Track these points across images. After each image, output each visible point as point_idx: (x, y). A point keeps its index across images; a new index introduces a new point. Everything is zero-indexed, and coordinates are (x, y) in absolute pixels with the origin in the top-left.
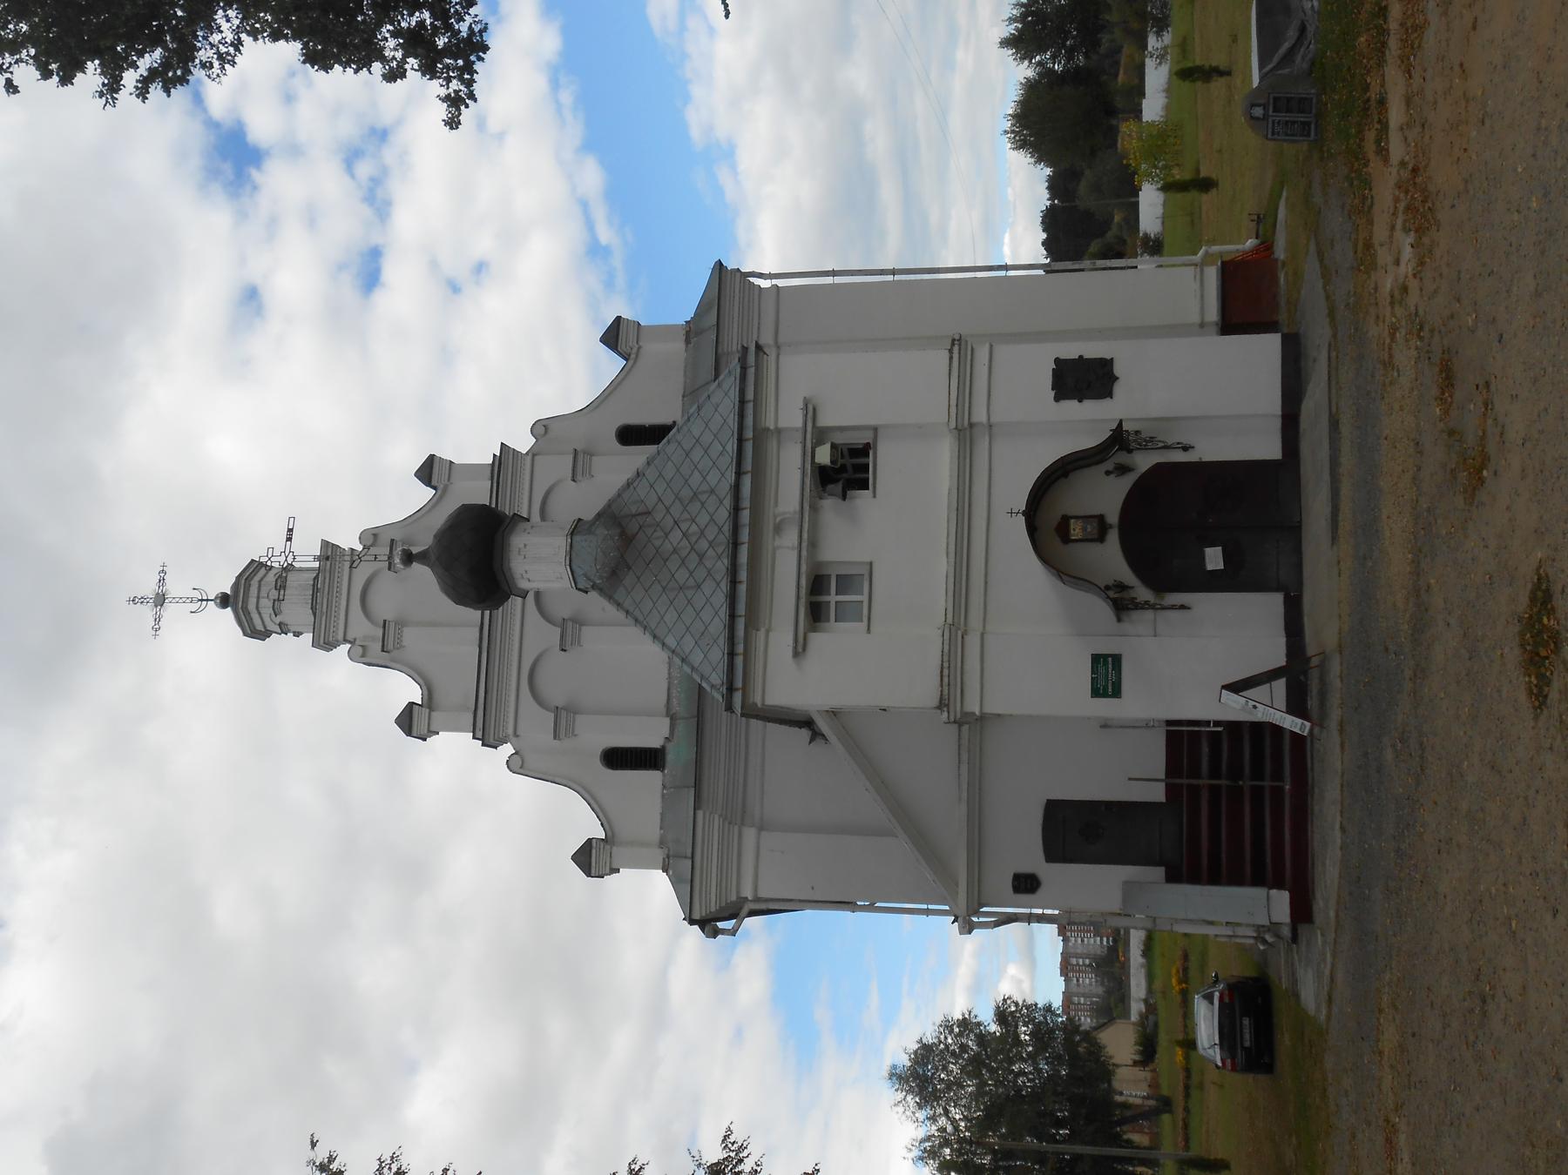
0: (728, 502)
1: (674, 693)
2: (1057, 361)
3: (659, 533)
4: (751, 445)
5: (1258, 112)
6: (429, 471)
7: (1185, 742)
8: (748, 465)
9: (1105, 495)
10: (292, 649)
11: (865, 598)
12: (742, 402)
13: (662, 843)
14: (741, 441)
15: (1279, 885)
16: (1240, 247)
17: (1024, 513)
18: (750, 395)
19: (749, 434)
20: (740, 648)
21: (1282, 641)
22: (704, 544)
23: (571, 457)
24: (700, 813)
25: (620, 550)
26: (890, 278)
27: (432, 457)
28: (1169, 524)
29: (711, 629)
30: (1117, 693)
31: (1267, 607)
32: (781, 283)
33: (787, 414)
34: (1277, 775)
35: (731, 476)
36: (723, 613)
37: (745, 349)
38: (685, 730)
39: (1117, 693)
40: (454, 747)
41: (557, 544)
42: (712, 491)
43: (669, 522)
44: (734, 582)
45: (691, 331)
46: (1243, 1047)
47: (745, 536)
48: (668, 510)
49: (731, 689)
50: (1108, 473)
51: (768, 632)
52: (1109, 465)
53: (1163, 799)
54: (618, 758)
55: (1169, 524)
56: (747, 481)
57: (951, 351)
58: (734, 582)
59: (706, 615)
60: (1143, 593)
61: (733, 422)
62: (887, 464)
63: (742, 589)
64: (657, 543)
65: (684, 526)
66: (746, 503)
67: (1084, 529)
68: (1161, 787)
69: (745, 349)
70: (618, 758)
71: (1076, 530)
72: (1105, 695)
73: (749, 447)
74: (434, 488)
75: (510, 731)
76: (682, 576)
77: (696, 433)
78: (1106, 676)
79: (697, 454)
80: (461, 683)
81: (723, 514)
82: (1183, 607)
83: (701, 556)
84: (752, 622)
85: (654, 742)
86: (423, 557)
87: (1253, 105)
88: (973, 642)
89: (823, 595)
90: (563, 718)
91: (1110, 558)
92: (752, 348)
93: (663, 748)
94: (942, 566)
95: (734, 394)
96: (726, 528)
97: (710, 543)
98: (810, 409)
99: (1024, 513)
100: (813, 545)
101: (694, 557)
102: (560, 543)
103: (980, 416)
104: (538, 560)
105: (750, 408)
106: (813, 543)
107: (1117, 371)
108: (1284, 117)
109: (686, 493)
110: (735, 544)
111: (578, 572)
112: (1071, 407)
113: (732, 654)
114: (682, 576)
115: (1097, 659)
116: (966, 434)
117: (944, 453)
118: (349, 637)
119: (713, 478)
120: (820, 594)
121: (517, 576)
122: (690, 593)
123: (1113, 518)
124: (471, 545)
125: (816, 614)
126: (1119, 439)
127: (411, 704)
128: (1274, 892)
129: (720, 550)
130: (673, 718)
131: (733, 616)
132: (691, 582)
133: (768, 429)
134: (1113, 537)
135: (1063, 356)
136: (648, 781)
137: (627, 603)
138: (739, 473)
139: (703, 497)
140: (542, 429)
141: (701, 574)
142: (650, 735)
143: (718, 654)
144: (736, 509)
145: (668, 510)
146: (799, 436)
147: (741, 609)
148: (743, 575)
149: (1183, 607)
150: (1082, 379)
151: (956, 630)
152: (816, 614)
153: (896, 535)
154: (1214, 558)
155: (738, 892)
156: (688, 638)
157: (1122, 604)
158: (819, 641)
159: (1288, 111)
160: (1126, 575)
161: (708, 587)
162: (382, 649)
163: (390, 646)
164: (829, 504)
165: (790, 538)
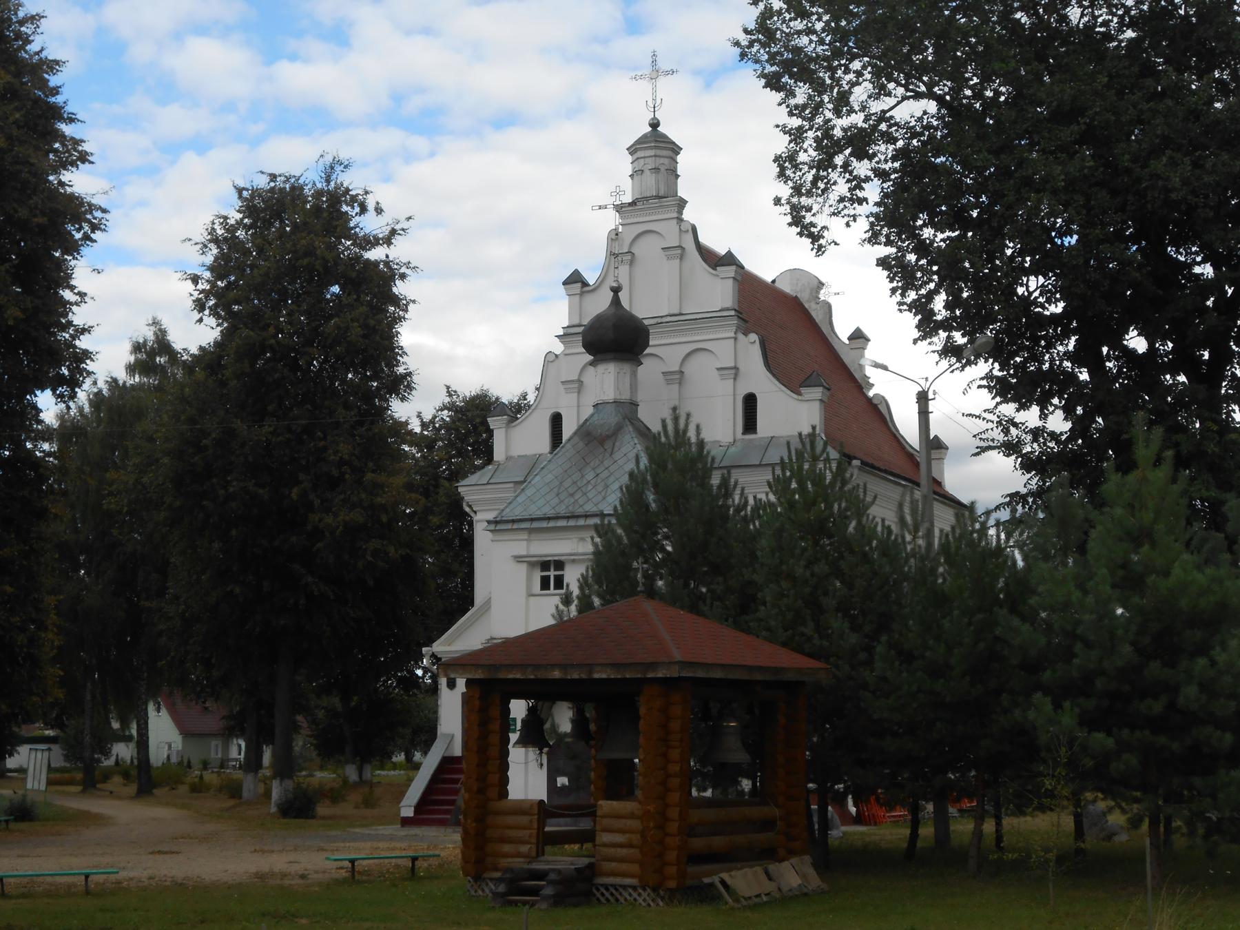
84: (531, 531)
86: (616, 301)
90: (578, 385)
136: (542, 443)
147: (536, 525)
154: (562, 781)
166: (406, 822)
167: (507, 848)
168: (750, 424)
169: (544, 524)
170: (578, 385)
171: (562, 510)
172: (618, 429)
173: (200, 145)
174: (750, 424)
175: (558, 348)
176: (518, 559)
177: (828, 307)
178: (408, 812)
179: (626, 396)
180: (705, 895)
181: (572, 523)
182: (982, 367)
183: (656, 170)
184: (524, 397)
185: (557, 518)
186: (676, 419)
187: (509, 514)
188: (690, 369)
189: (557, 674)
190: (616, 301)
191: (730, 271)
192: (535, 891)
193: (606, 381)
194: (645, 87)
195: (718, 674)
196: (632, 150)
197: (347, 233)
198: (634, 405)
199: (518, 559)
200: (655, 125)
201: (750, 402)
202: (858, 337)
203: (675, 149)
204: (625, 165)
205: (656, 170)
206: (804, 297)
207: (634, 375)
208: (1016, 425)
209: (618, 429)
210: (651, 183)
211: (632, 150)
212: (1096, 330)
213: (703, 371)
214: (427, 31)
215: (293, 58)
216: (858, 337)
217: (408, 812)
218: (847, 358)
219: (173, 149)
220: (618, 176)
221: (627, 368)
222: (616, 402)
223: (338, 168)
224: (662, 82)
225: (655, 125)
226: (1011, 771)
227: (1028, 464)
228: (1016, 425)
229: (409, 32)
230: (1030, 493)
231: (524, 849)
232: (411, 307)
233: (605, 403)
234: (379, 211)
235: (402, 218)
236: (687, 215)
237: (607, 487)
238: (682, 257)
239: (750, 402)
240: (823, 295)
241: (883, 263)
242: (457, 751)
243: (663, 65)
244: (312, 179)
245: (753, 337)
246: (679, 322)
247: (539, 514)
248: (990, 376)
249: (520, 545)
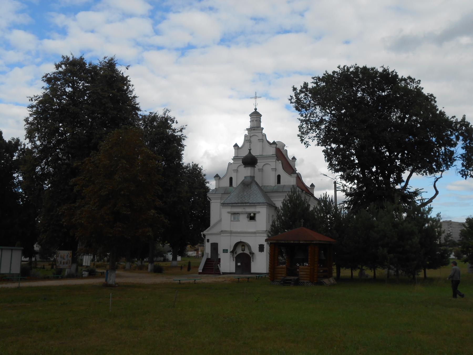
9: (247, 251)
13: (219, 187)
30: (227, 250)
31: (233, 270)
33: (258, 209)
46: (26, 273)
54: (231, 179)
60: (235, 255)
62: (252, 222)
70: (231, 179)
71: (243, 247)
78: (225, 251)
84: (232, 206)
86: (250, 153)
90: (237, 171)
94: (239, 230)
98: (259, 212)
106: (242, 213)
115: (227, 250)
123: (244, 252)
126: (252, 254)
134: (242, 252)
136: (228, 184)
147: (233, 205)
154: (239, 264)
157: (233, 252)
164: (246, 215)
165: (244, 210)
166: (200, 273)
167: (279, 275)
168: (279, 181)
169: (235, 205)
170: (237, 171)
171: (239, 201)
172: (251, 183)
173: (20, 65)
174: (279, 181)
175: (232, 162)
176: (228, 212)
177: (286, 151)
178: (201, 271)
179: (252, 175)
180: (321, 284)
181: (242, 205)
182: (340, 173)
183: (257, 121)
184: (189, 164)
185: (238, 203)
186: (326, 196)
187: (226, 202)
188: (264, 168)
189: (292, 242)
190: (250, 153)
191: (275, 146)
192: (290, 283)
193: (246, 172)
194: (253, 100)
195: (323, 242)
196: (250, 115)
197: (169, 127)
198: (254, 177)
199: (228, 212)
200: (256, 109)
201: (279, 177)
202: (294, 158)
203: (261, 116)
204: (249, 119)
205: (257, 121)
206: (281, 148)
207: (254, 170)
208: (346, 186)
209: (251, 183)
210: (255, 124)
211: (250, 115)
212: (364, 166)
213: (268, 169)
214: (92, 31)
215: (49, 38)
216: (294, 158)
217: (201, 271)
218: (291, 163)
219: (11, 66)
220: (246, 123)
221: (253, 168)
222: (251, 177)
223: (167, 112)
224: (258, 99)
225: (256, 109)
226: (374, 262)
227: (347, 195)
228: (346, 186)
229: (87, 31)
230: (348, 201)
231: (283, 275)
232: (185, 147)
233: (248, 176)
234: (177, 123)
235: (185, 125)
236: (264, 132)
237: (250, 196)
238: (263, 142)
239: (279, 177)
240: (285, 148)
241: (323, 151)
242: (209, 257)
243: (258, 95)
244: (160, 113)
245: (280, 161)
246: (262, 157)
247: (234, 202)
248: (341, 175)
249: (229, 209)
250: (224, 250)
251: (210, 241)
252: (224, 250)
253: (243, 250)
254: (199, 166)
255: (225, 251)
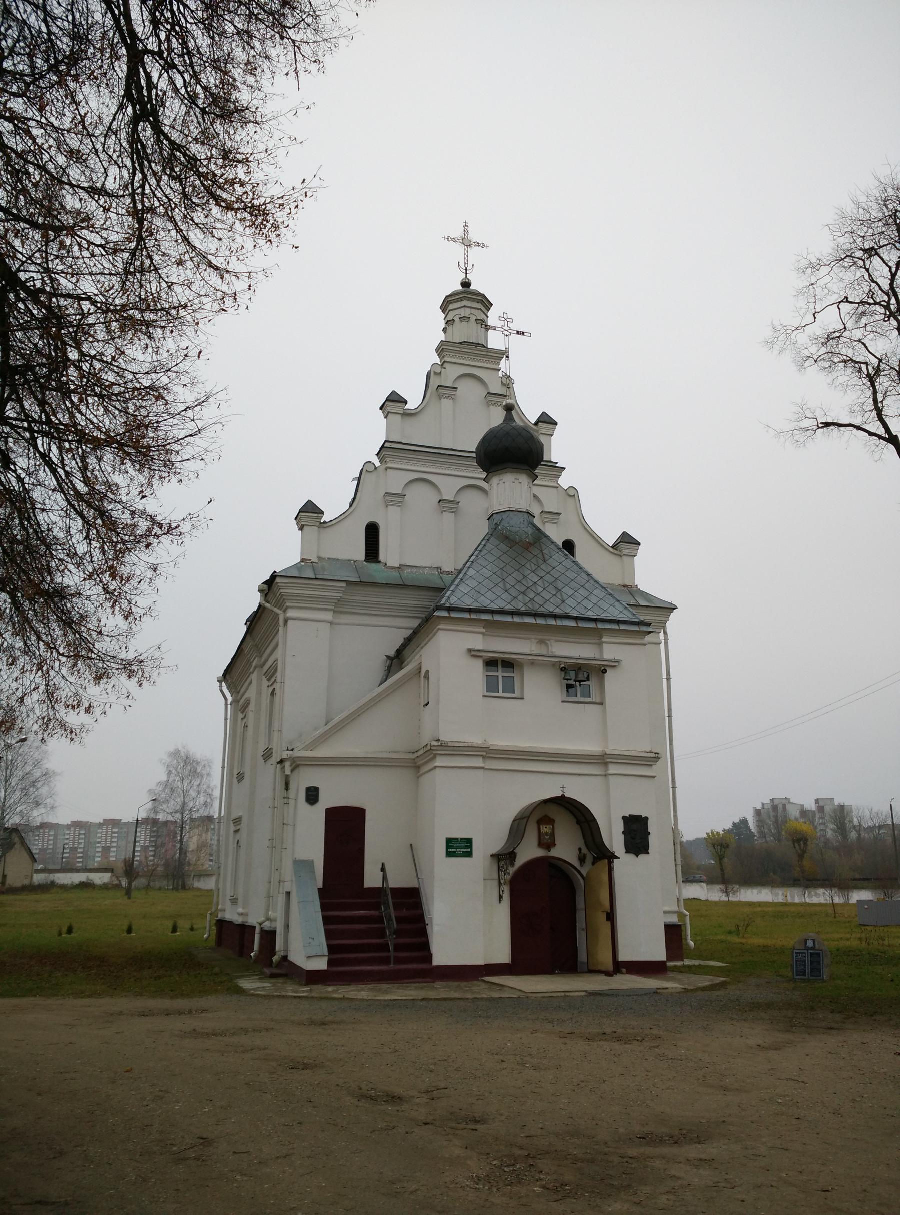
0: (558, 611)
1: (415, 570)
2: (647, 818)
3: (534, 568)
4: (593, 627)
5: (810, 944)
6: (546, 420)
7: (411, 902)
8: (582, 624)
9: (567, 848)
10: (433, 329)
11: (501, 694)
12: (619, 622)
14: (596, 620)
15: (330, 963)
16: (689, 937)
17: (563, 795)
18: (623, 627)
19: (600, 625)
20: (474, 616)
21: (480, 962)
22: (532, 595)
23: (556, 511)
24: (344, 585)
25: (521, 543)
26: (667, 714)
27: (556, 424)
28: (554, 891)
29: (483, 598)
30: (449, 854)
32: (663, 645)
33: (611, 650)
34: (398, 961)
35: (574, 613)
36: (493, 606)
37: (649, 624)
38: (394, 578)
39: (449, 854)
40: (376, 430)
41: (522, 504)
42: (563, 602)
43: (543, 574)
44: (512, 613)
45: (631, 589)
47: (541, 621)
48: (549, 573)
49: (449, 609)
50: (580, 849)
51: (483, 634)
52: (585, 850)
53: (365, 886)
54: (372, 532)
55: (554, 891)
56: (572, 623)
57: (651, 752)
58: (512, 613)
59: (489, 595)
61: (605, 615)
63: (509, 618)
64: (528, 566)
65: (540, 583)
66: (560, 622)
67: (547, 834)
68: (378, 884)
69: (649, 624)
70: (372, 532)
71: (546, 829)
72: (448, 847)
73: (592, 625)
74: (536, 424)
75: (389, 465)
76: (511, 581)
77: (595, 592)
78: (459, 847)
79: (582, 592)
80: (419, 434)
81: (551, 608)
82: (501, 897)
83: (524, 593)
84: (488, 624)
85: (382, 557)
86: (509, 418)
87: (814, 941)
88: (479, 762)
89: (500, 666)
91: (529, 851)
92: (650, 629)
93: (380, 562)
95: (621, 617)
96: (590, 613)
97: (532, 599)
98: (615, 664)
99: (563, 795)
100: (533, 663)
101: (523, 589)
102: (522, 505)
103: (613, 769)
104: (510, 491)
105: (615, 626)
107: (642, 857)
108: (808, 959)
109: (560, 585)
110: (535, 615)
111: (505, 516)
112: (619, 827)
113: (470, 611)
114: (511, 581)
115: (469, 841)
116: (603, 760)
117: (593, 747)
118: (446, 365)
119: (570, 601)
120: (503, 667)
121: (501, 477)
122: (501, 585)
123: (555, 853)
124: (516, 449)
125: (491, 663)
127: (406, 402)
128: (327, 958)
129: (530, 605)
130: (401, 568)
131: (493, 612)
132: (508, 587)
133: (601, 637)
135: (649, 822)
136: (360, 554)
137: (490, 546)
138: (576, 618)
139: (559, 595)
140: (572, 494)
141: (514, 593)
142: (389, 553)
143: (468, 602)
144: (556, 616)
145: (549, 573)
146: (597, 656)
147: (498, 617)
148: (517, 619)
149: (501, 897)
150: (637, 833)
151: (487, 753)
152: (491, 663)
153: (538, 716)
155: (291, 607)
156: (475, 584)
157: (504, 858)
158: (478, 665)
159: (812, 962)
160: (520, 861)
161: (505, 596)
162: (437, 388)
163: (441, 391)
176: (473, 653)
199: (473, 653)
225: (466, 284)
250: (450, 841)
251: (322, 795)
252: (450, 841)
253: (547, 843)
254: (850, 209)
255: (459, 847)
